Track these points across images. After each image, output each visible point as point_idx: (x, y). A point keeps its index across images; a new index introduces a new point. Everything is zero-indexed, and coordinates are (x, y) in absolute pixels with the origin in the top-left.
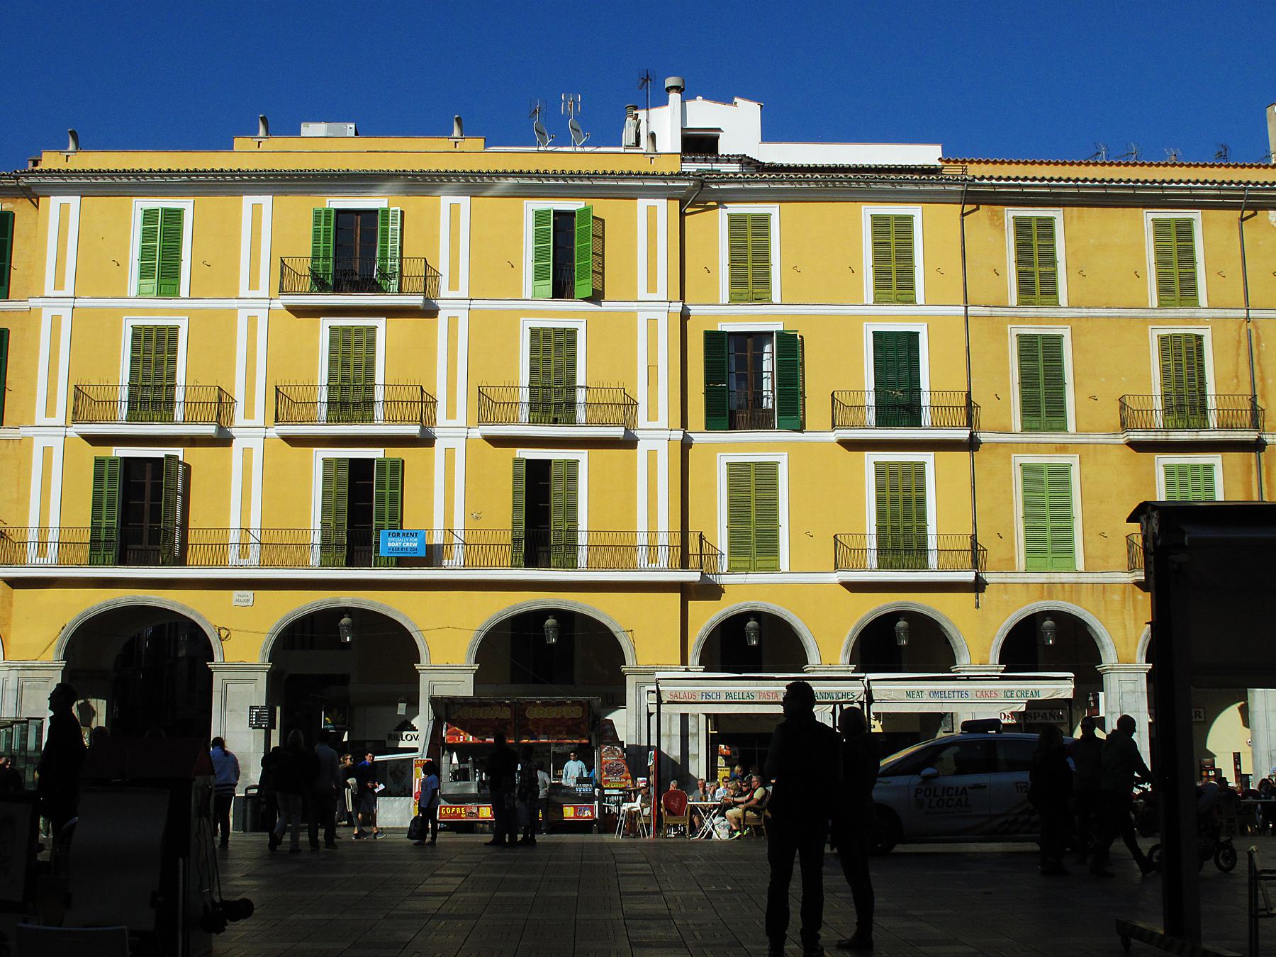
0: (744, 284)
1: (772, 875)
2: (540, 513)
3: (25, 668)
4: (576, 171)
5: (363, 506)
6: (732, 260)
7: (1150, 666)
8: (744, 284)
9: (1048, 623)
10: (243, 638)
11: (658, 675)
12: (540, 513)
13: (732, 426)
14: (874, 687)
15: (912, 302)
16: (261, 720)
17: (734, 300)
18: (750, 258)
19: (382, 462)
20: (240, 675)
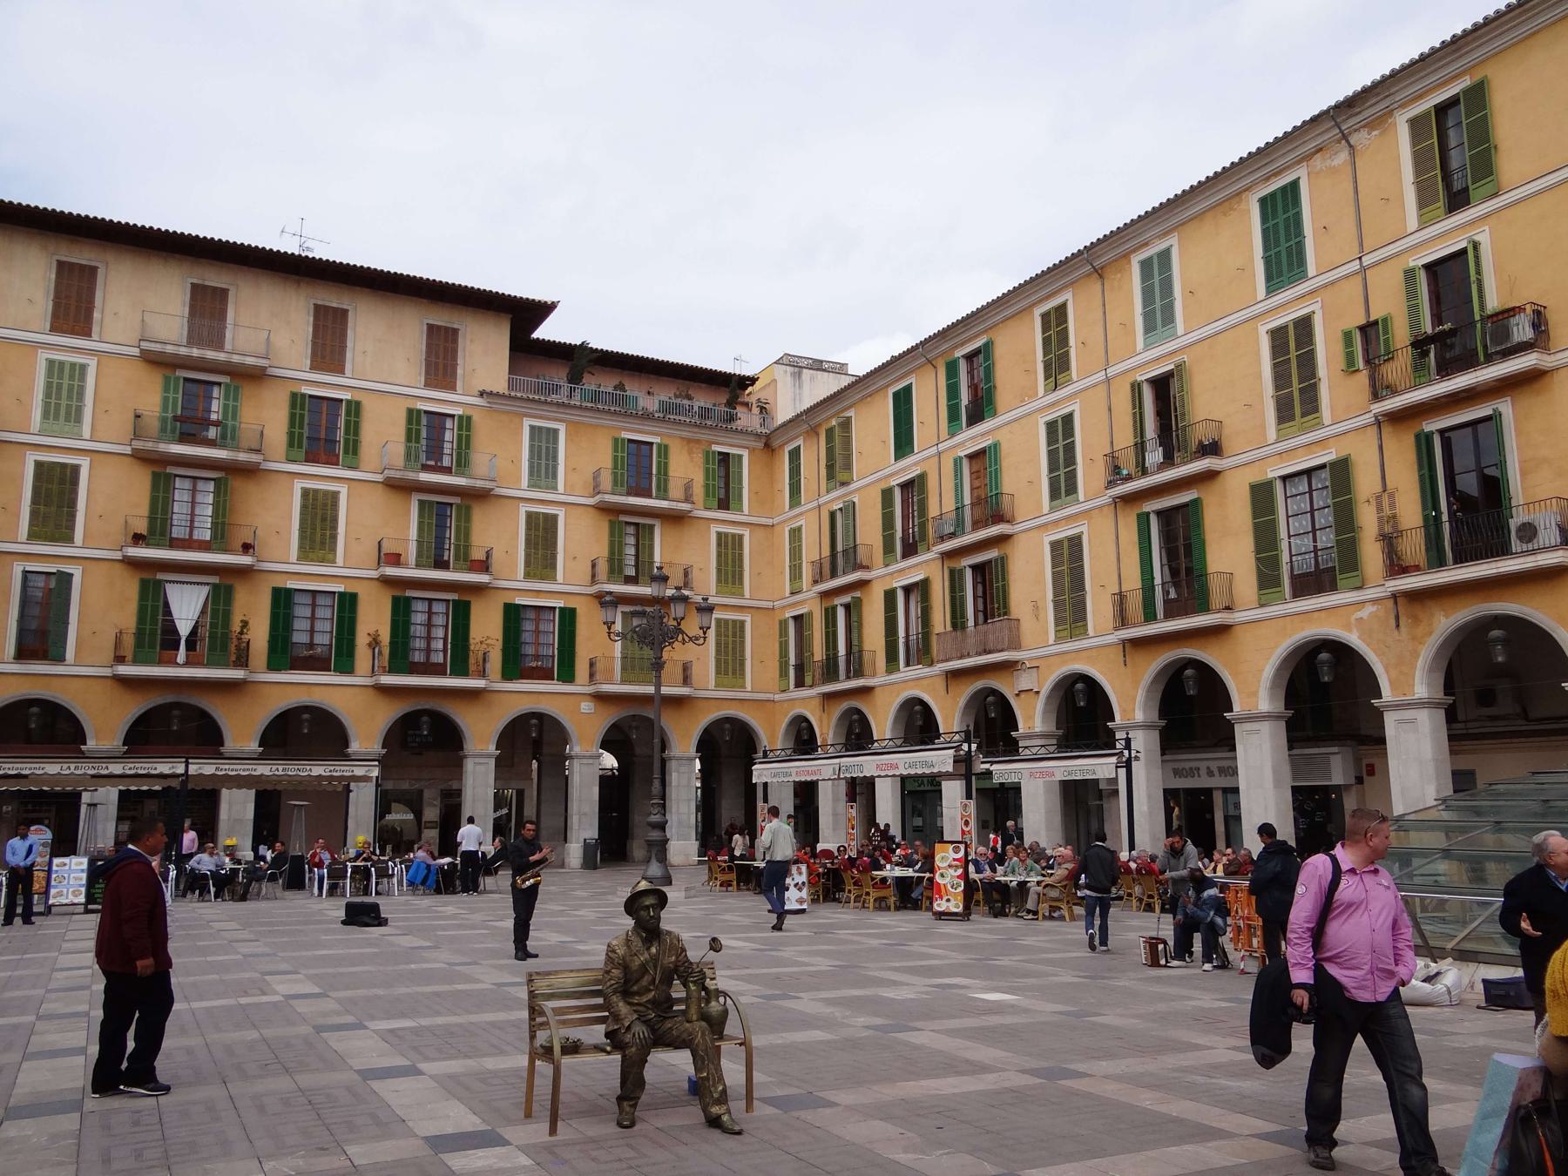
7: (1450, 699)
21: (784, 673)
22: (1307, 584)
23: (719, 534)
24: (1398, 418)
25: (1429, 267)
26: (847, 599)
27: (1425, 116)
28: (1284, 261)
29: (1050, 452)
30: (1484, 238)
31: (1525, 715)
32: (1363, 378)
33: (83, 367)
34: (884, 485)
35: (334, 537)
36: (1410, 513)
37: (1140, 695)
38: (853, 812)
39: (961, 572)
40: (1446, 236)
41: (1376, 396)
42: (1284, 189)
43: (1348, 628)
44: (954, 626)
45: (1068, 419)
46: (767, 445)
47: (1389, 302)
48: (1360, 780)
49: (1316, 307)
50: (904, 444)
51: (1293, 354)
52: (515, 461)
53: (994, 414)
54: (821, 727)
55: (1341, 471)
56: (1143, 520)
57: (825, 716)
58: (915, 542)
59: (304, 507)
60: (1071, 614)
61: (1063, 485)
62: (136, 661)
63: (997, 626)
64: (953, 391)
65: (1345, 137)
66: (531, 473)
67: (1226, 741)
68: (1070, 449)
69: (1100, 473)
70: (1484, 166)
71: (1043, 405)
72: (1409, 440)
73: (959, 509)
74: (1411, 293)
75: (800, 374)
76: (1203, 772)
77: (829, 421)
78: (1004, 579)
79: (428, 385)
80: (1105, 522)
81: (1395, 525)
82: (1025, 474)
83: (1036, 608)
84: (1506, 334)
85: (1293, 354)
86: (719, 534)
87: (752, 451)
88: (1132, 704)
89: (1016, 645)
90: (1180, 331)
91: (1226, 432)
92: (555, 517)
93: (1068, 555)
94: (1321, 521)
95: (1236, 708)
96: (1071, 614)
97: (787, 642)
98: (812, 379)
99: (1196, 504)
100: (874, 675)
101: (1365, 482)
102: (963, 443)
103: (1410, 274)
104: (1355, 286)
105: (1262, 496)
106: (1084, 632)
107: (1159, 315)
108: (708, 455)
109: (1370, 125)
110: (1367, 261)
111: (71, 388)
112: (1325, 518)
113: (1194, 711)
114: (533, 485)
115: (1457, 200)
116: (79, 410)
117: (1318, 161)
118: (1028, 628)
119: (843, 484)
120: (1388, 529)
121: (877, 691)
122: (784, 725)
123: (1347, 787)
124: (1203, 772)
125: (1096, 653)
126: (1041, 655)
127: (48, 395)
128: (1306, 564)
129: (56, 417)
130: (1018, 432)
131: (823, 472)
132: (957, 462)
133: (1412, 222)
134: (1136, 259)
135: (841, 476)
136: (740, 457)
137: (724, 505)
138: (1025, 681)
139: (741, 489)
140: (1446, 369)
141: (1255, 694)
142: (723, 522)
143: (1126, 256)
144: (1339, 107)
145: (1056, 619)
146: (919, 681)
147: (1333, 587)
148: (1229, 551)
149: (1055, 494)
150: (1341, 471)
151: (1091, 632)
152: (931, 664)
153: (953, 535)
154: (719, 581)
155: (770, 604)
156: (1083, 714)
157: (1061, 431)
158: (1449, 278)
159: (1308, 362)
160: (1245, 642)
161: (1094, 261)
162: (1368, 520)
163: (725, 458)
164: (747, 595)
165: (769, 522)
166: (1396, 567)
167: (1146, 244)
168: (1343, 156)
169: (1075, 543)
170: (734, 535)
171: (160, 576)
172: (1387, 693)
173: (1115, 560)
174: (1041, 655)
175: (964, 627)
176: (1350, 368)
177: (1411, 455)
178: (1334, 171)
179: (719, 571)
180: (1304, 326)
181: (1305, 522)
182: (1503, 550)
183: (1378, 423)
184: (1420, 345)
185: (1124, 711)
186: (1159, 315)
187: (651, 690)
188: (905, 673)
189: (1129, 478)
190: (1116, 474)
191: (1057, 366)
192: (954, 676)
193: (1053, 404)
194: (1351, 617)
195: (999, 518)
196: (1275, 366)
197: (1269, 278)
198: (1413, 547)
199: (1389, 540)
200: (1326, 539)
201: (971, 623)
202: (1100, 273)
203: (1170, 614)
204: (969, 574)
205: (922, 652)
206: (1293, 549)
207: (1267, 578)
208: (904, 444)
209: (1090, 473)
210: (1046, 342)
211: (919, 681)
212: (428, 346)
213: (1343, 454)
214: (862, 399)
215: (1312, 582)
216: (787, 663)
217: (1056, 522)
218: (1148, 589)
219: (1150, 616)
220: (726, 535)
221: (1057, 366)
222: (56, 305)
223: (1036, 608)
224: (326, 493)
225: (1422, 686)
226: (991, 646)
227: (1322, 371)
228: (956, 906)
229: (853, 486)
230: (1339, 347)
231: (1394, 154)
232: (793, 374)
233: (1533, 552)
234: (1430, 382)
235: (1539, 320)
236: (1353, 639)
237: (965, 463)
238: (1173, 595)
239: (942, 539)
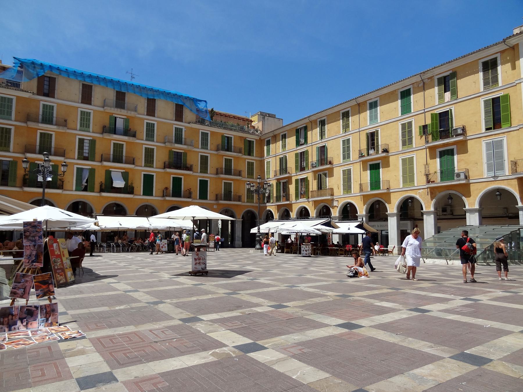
17: (201, 172)
26: (285, 181)
31: (452, 214)
33: (90, 113)
35: (153, 161)
42: (407, 90)
43: (416, 194)
45: (348, 140)
52: (198, 141)
58: (304, 168)
59: (145, 152)
60: (347, 187)
61: (346, 155)
62: (224, 200)
65: (422, 80)
66: (202, 145)
67: (386, 220)
69: (357, 155)
75: (264, 118)
76: (376, 226)
79: (176, 120)
81: (428, 172)
82: (335, 153)
85: (407, 130)
90: (379, 122)
92: (207, 156)
95: (389, 212)
96: (347, 187)
98: (267, 119)
107: (374, 118)
111: (87, 119)
114: (202, 148)
116: (89, 125)
120: (427, 173)
124: (376, 226)
127: (81, 120)
129: (83, 127)
141: (393, 208)
146: (303, 203)
157: (346, 143)
159: (410, 132)
171: (110, 169)
180: (410, 124)
187: (47, 190)
188: (301, 200)
190: (361, 156)
192: (315, 202)
196: (402, 132)
209: (354, 155)
211: (303, 203)
212: (176, 109)
222: (82, 96)
224: (151, 149)
227: (414, 135)
233: (459, 180)
239: (313, 167)
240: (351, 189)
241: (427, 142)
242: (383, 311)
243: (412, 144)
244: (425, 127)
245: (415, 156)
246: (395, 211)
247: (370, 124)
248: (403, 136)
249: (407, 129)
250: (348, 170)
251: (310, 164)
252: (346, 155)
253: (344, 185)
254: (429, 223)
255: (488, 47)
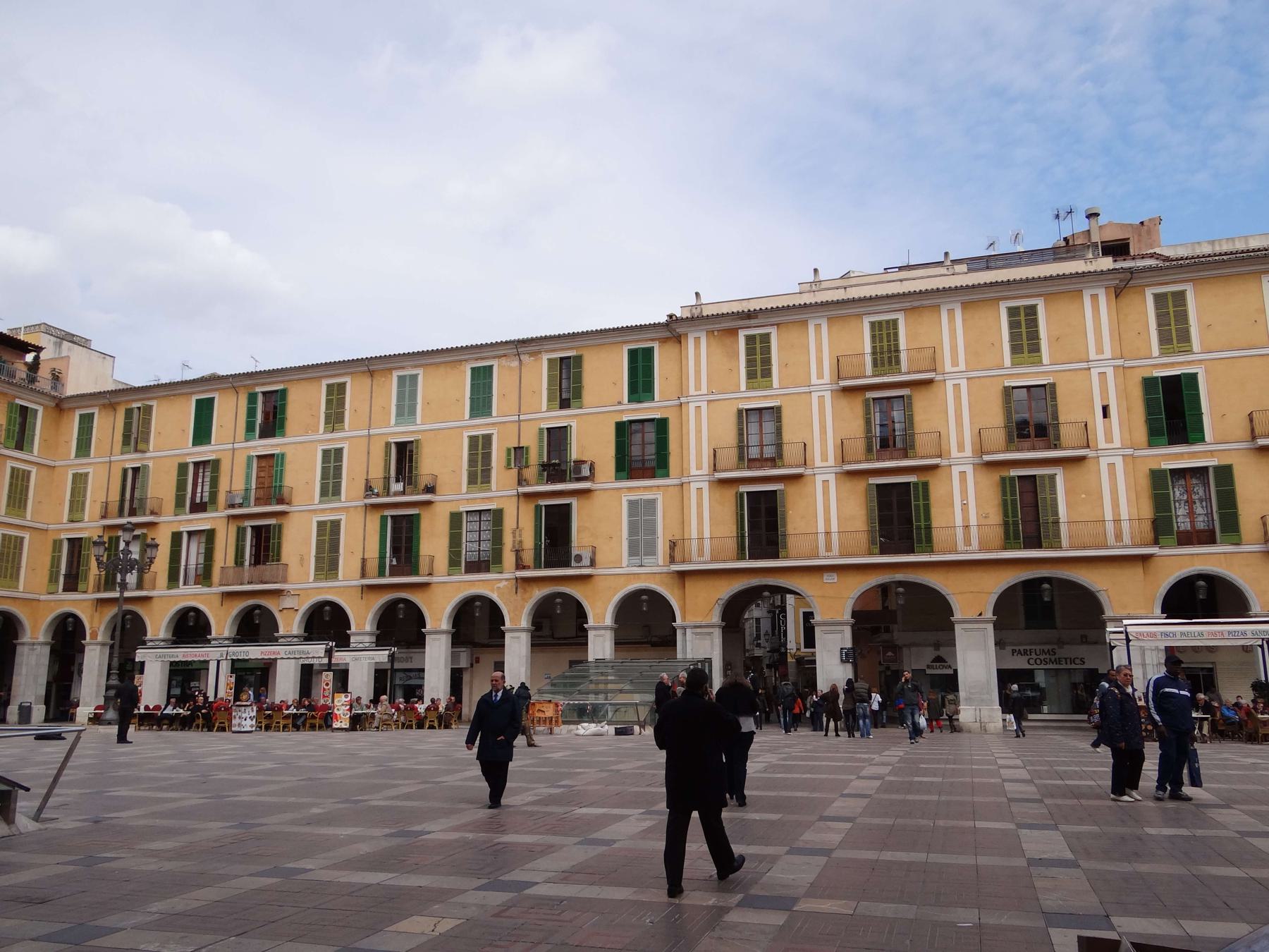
0: (1170, 341)
1: (745, 758)
2: (1026, 512)
3: (696, 627)
4: (1067, 272)
5: (899, 514)
6: (1159, 325)
8: (1170, 341)
9: (327, 608)
10: (834, 604)
11: (1125, 622)
12: (1026, 512)
13: (631, 477)
14: (1130, 629)
15: (1190, 351)
16: (847, 656)
18: (1173, 323)
19: (916, 484)
20: (833, 628)
21: (53, 578)
22: (474, 567)
23: (13, 469)
24: (528, 496)
25: (548, 429)
27: (555, 359)
28: (481, 404)
29: (323, 468)
30: (574, 424)
31: (552, 636)
32: (514, 472)
34: (182, 460)
36: (529, 542)
37: (370, 616)
38: (233, 680)
39: (244, 529)
40: (558, 418)
41: (520, 483)
43: (492, 591)
44: (236, 563)
45: (339, 452)
46: (57, 405)
47: (530, 440)
48: (472, 665)
49: (494, 432)
50: (202, 433)
51: (480, 451)
53: (283, 435)
54: (91, 622)
55: (498, 515)
56: (384, 519)
57: (97, 615)
60: (328, 562)
61: (331, 487)
63: (267, 569)
64: (251, 413)
68: (338, 469)
69: (98, 511)
70: (578, 394)
71: (323, 439)
72: (532, 507)
73: (247, 490)
74: (541, 440)
77: (133, 407)
78: (279, 538)
80: (358, 517)
82: (302, 476)
83: (302, 560)
84: (580, 471)
86: (13, 469)
87: (46, 407)
88: (362, 620)
89: (285, 581)
91: (439, 482)
93: (329, 534)
94: (484, 536)
96: (328, 562)
97: (59, 558)
99: (418, 515)
100: (154, 588)
101: (509, 523)
102: (255, 447)
103: (541, 430)
104: (515, 427)
105: (456, 519)
106: (336, 577)
107: (406, 408)
108: (11, 405)
109: (532, 354)
110: (522, 417)
112: (486, 535)
113: (401, 626)
115: (565, 404)
117: (504, 361)
118: (294, 570)
119: (144, 452)
121: (155, 601)
122: (49, 619)
123: (466, 669)
125: (344, 589)
126: (300, 584)
128: (474, 557)
130: (302, 447)
131: (119, 437)
132: (250, 458)
133: (544, 408)
134: (395, 374)
135: (140, 446)
136: (36, 411)
137: (19, 446)
138: (288, 602)
139: (33, 436)
140: (552, 479)
141: (440, 620)
142: (17, 459)
143: (390, 370)
144: (519, 341)
145: (316, 570)
146: (190, 595)
147: (487, 570)
148: (433, 543)
149: (324, 493)
150: (498, 515)
151: (340, 577)
152: (210, 586)
153: (241, 506)
154: (8, 505)
155: (45, 527)
156: (327, 623)
157: (333, 459)
158: (557, 438)
159: (487, 457)
160: (436, 592)
161: (372, 367)
162: (508, 540)
163: (24, 410)
164: (29, 518)
165: (52, 464)
166: (520, 566)
167: (403, 368)
168: (515, 364)
169: (336, 525)
170: (24, 471)
172: (508, 624)
173: (362, 540)
174: (300, 584)
175: (242, 564)
176: (508, 467)
177: (532, 514)
178: (510, 368)
179: (9, 497)
180: (487, 438)
181: (476, 536)
182: (567, 564)
183: (518, 495)
184: (544, 466)
185: (358, 625)
186: (406, 408)
189: (378, 495)
191: (335, 418)
193: (329, 440)
194: (493, 585)
195: (281, 501)
196: (470, 455)
197: (472, 409)
198: (528, 557)
199: (518, 552)
200: (486, 546)
201: (247, 563)
202: (372, 373)
203: (392, 574)
204: (249, 531)
205: (205, 576)
206: (469, 549)
207: (454, 562)
208: (202, 433)
210: (329, 402)
213: (500, 507)
214: (164, 396)
215: (476, 567)
216: (58, 572)
217: (323, 510)
218: (382, 557)
219: (381, 574)
220: (18, 469)
221: (335, 418)
223: (302, 559)
225: (525, 622)
226: (266, 579)
228: (346, 724)
229: (148, 455)
230: (504, 454)
231: (539, 373)
232: (55, 343)
233: (828, 557)
234: (542, 484)
235: (592, 468)
236: (495, 597)
237: (255, 461)
238: (394, 563)
239: (232, 506)
240: (337, 569)
241: (521, 481)
242: (293, 822)
243: (489, 482)
244: (520, 451)
245: (343, 517)
246: (609, 620)
247: (397, 424)
248: (472, 461)
249: (480, 448)
250: (332, 522)
251: (222, 498)
252: (331, 487)
253: (318, 559)
254: (600, 646)
255: (901, 281)
